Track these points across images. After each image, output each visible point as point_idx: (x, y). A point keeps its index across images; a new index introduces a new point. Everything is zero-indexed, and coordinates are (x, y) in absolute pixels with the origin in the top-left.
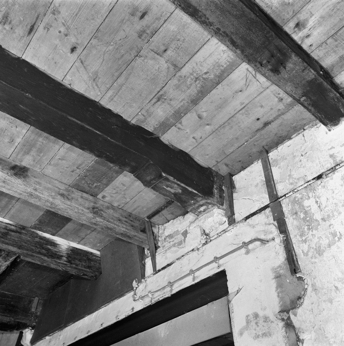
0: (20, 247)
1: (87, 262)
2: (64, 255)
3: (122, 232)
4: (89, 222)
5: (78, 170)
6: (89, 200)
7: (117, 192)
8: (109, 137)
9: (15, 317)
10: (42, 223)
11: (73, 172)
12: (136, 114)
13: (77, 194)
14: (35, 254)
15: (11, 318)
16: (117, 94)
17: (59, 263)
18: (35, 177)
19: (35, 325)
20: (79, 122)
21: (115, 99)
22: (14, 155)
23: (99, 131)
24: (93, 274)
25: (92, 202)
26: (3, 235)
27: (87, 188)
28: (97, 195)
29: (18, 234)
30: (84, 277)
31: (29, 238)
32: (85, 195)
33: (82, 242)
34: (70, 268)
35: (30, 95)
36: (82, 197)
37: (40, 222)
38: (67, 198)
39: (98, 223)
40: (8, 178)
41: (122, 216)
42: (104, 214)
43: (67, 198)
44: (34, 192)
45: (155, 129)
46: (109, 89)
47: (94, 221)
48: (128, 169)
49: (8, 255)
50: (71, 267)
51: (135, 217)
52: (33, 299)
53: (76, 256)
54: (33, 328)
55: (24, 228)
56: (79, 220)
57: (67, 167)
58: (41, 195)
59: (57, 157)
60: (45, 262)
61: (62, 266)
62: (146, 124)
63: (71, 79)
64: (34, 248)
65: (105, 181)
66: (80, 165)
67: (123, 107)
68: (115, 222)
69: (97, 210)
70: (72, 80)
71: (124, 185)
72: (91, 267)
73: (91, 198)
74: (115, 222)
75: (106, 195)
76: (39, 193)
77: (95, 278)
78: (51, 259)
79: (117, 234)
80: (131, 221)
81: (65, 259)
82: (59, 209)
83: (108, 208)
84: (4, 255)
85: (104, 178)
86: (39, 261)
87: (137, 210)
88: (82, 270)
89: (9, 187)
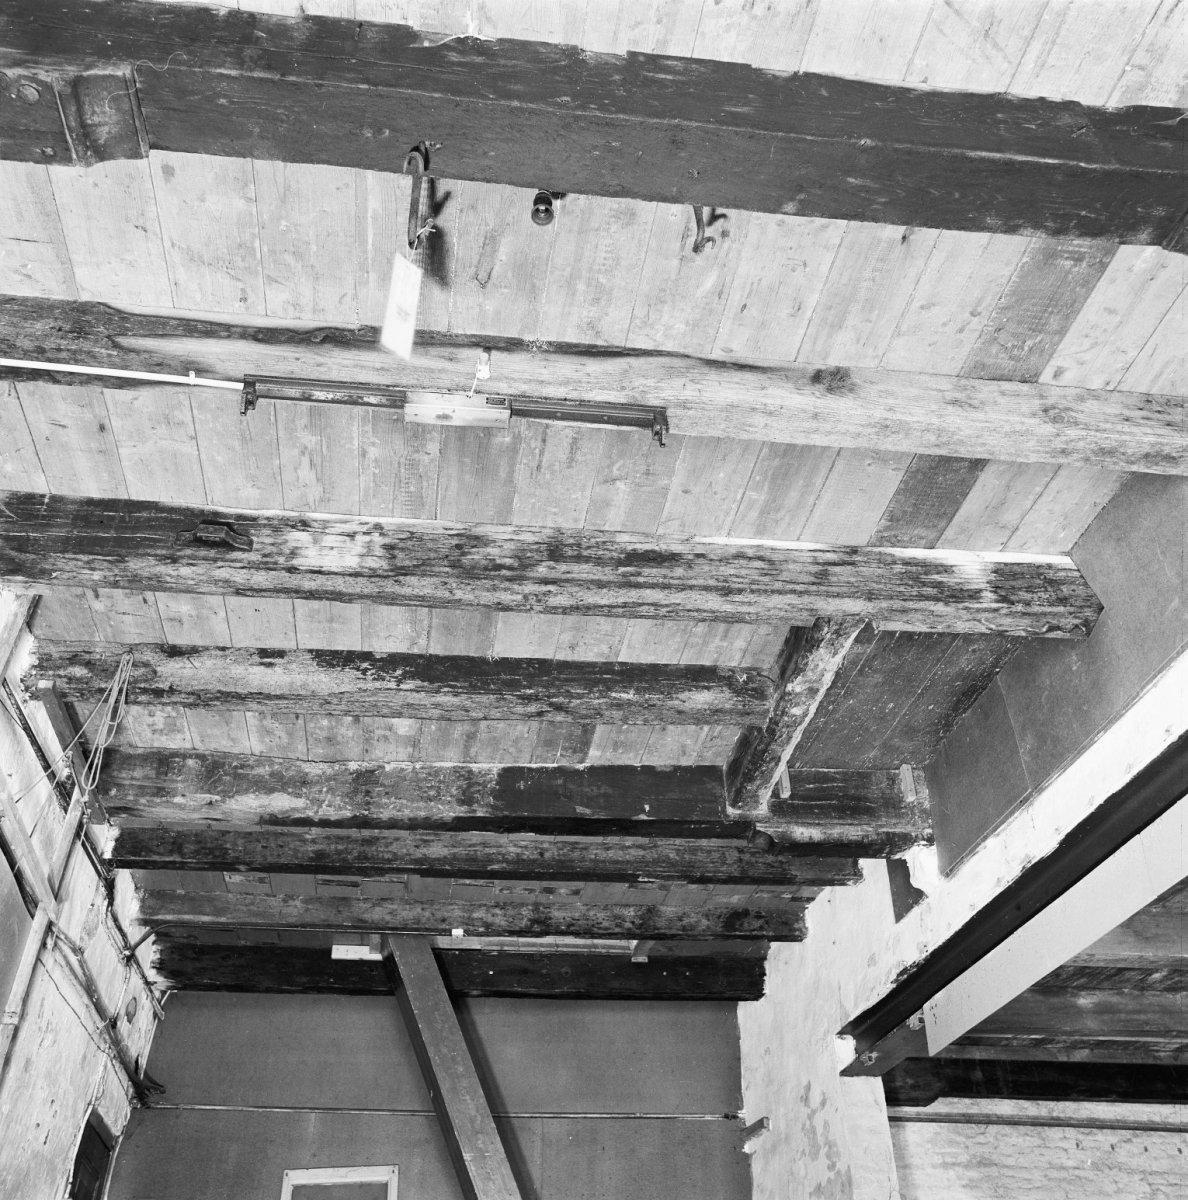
0: (870, 596)
1: (1049, 589)
2: (982, 586)
3: (1147, 449)
4: (1047, 453)
5: (976, 319)
6: (1022, 394)
7: (1096, 343)
8: (1081, 161)
9: (874, 824)
10: (898, 520)
11: (961, 331)
12: (1117, 75)
13: (988, 390)
14: (911, 603)
15: (865, 827)
16: (1054, 42)
17: (978, 610)
18: (872, 383)
19: (932, 835)
20: (998, 155)
21: (1051, 61)
22: (807, 347)
23: (1051, 157)
24: (1076, 617)
25: (1033, 396)
26: (818, 578)
27: (1007, 364)
28: (1037, 375)
29: (849, 567)
30: (1051, 635)
31: (880, 571)
32: (1006, 386)
33: (1011, 544)
34: (1009, 620)
35: (869, 142)
36: (1003, 393)
37: (891, 520)
38: (970, 405)
39: (1071, 446)
40: (820, 403)
41: (1127, 407)
42: (1081, 417)
43: (970, 405)
44: (889, 415)
45: (1182, 92)
46: (1028, 41)
47: (1058, 444)
48: (1144, 236)
49: (837, 633)
50: (1010, 614)
51: (1165, 401)
52: (897, 771)
53: (1013, 583)
54: (930, 840)
55: (854, 551)
56: (1019, 456)
57: (944, 324)
58: (909, 419)
59: (916, 304)
60: (940, 619)
61: (987, 620)
62: (1153, 90)
63: (924, 63)
64: (902, 589)
65: (1054, 323)
66: (979, 302)
67: (1076, 73)
68: (1119, 427)
69: (1057, 411)
70: (927, 65)
71: (1111, 311)
72: (1066, 599)
73: (1025, 387)
74: (1119, 427)
75: (1065, 365)
76: (903, 413)
77: (1084, 629)
78: (954, 605)
79: (1133, 463)
80: (1159, 412)
81: (989, 595)
82: (961, 442)
83: (1081, 399)
84: (828, 636)
85: (1052, 312)
86: (924, 622)
87: (1164, 376)
88: (1044, 614)
89: (828, 427)
